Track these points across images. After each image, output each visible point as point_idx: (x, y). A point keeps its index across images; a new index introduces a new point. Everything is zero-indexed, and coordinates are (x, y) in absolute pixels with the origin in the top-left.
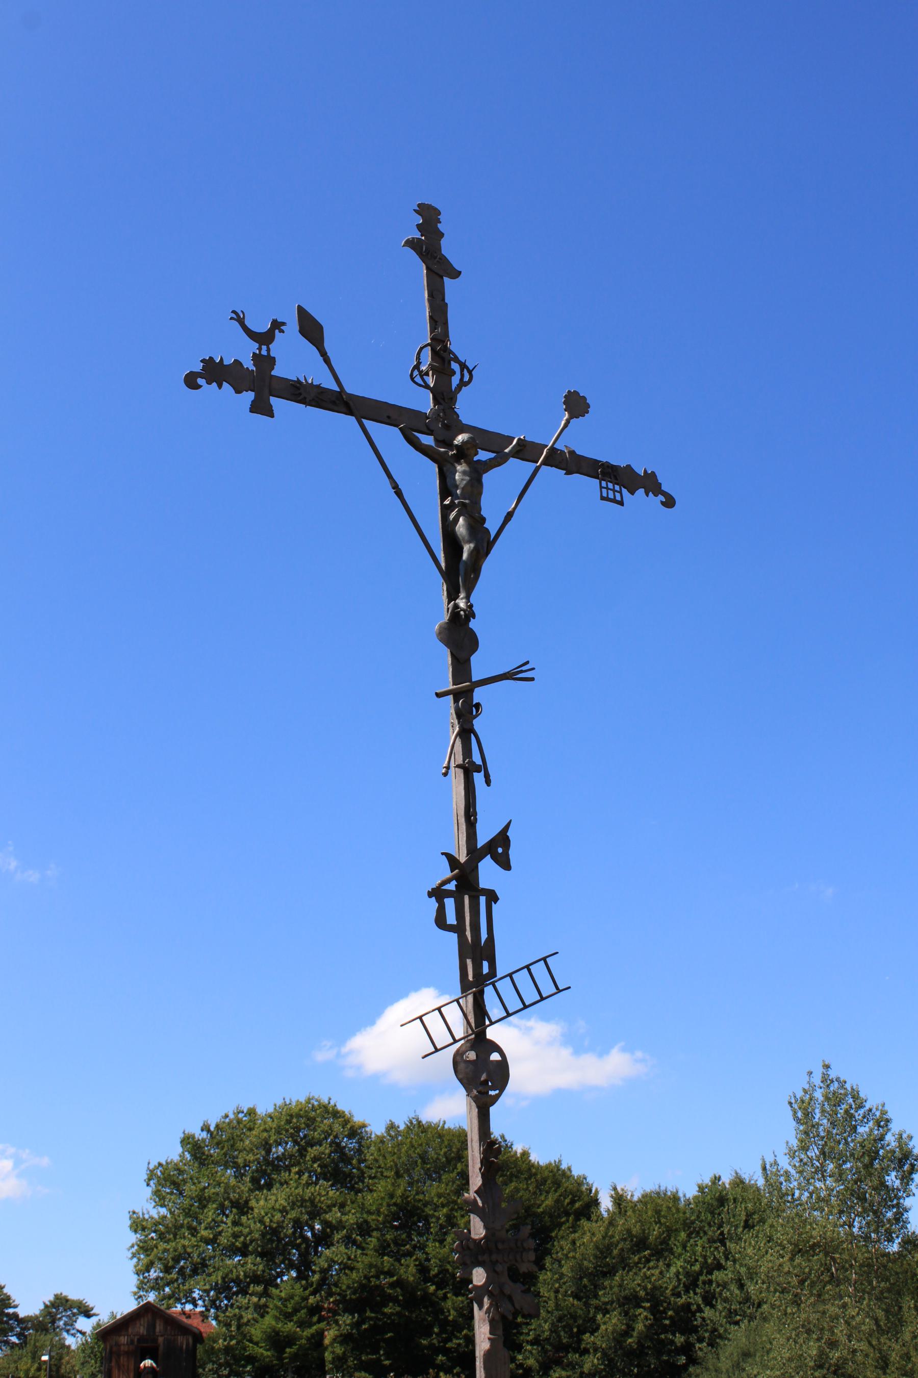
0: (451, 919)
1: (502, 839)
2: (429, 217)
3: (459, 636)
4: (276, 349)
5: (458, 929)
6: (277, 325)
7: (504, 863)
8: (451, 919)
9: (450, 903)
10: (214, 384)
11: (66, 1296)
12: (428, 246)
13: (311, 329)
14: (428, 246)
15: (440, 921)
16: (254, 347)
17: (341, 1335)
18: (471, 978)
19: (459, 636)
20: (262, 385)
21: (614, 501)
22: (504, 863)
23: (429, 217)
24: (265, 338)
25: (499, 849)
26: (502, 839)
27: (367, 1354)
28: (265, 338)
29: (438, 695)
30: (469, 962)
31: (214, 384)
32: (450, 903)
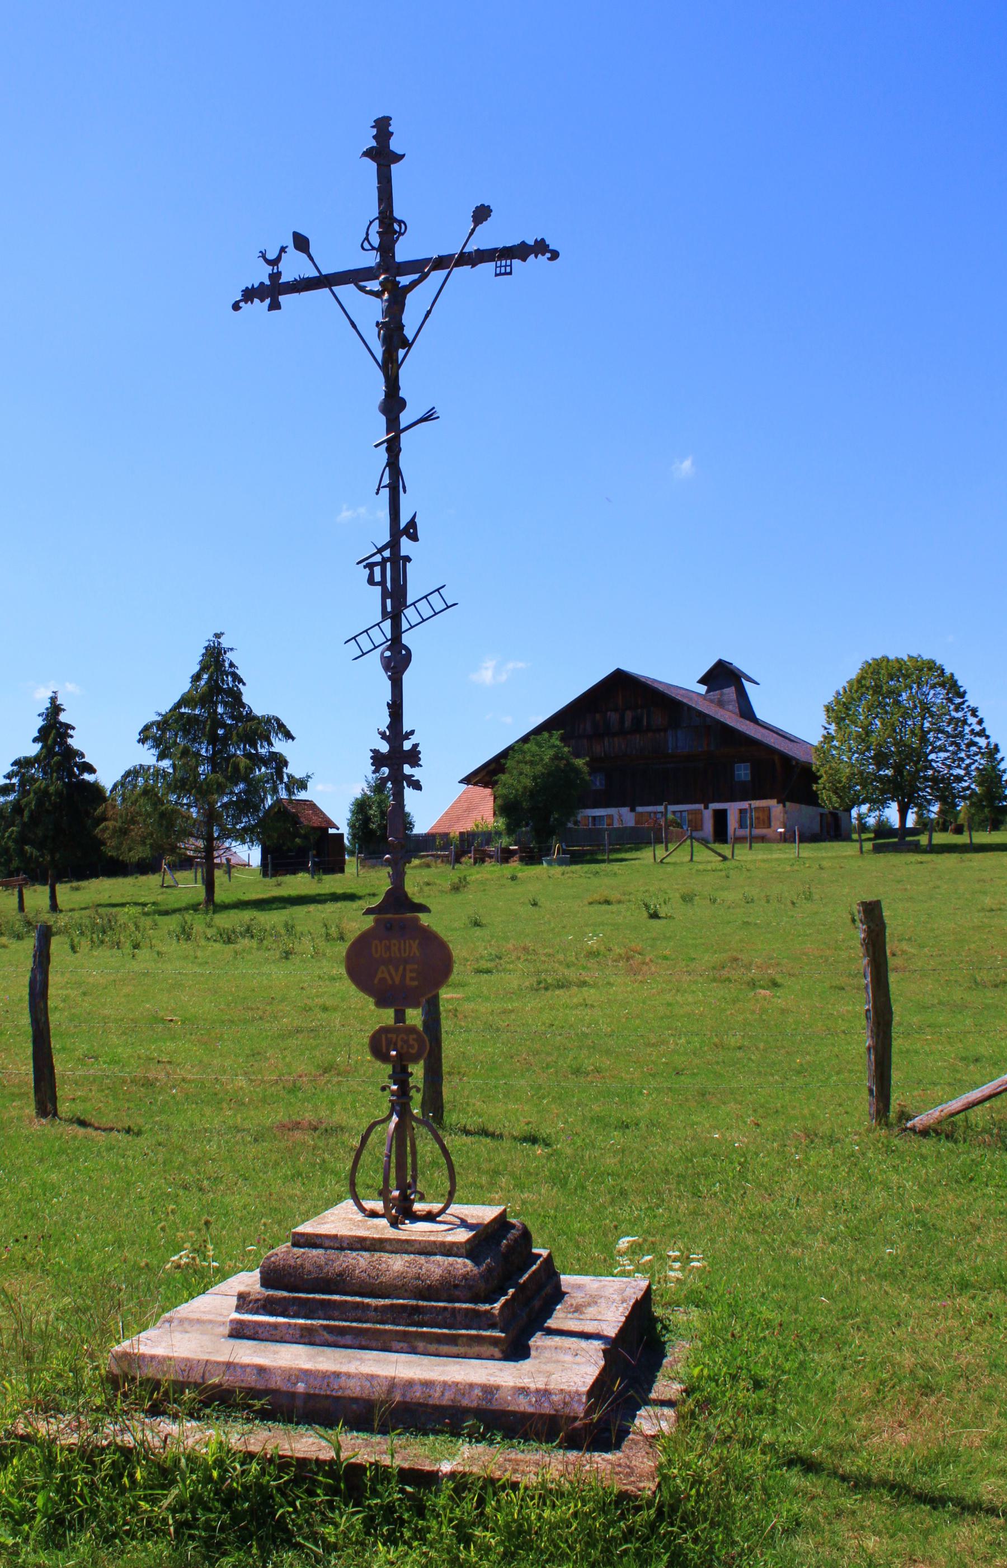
0: (378, 578)
1: (412, 523)
2: (383, 127)
3: (393, 404)
4: (282, 266)
5: (383, 583)
6: (283, 250)
7: (414, 538)
8: (378, 578)
9: (377, 570)
10: (373, 768)
11: (353, 812)
12: (383, 155)
13: (301, 243)
14: (383, 155)
15: (371, 581)
16: (269, 269)
17: (285, 808)
18: (389, 609)
19: (393, 404)
20: (272, 292)
21: (506, 274)
22: (414, 538)
23: (383, 127)
24: (275, 262)
25: (411, 531)
26: (412, 523)
27: (886, 775)
28: (275, 262)
29: (377, 493)
30: (389, 601)
31: (373, 768)
32: (377, 570)
